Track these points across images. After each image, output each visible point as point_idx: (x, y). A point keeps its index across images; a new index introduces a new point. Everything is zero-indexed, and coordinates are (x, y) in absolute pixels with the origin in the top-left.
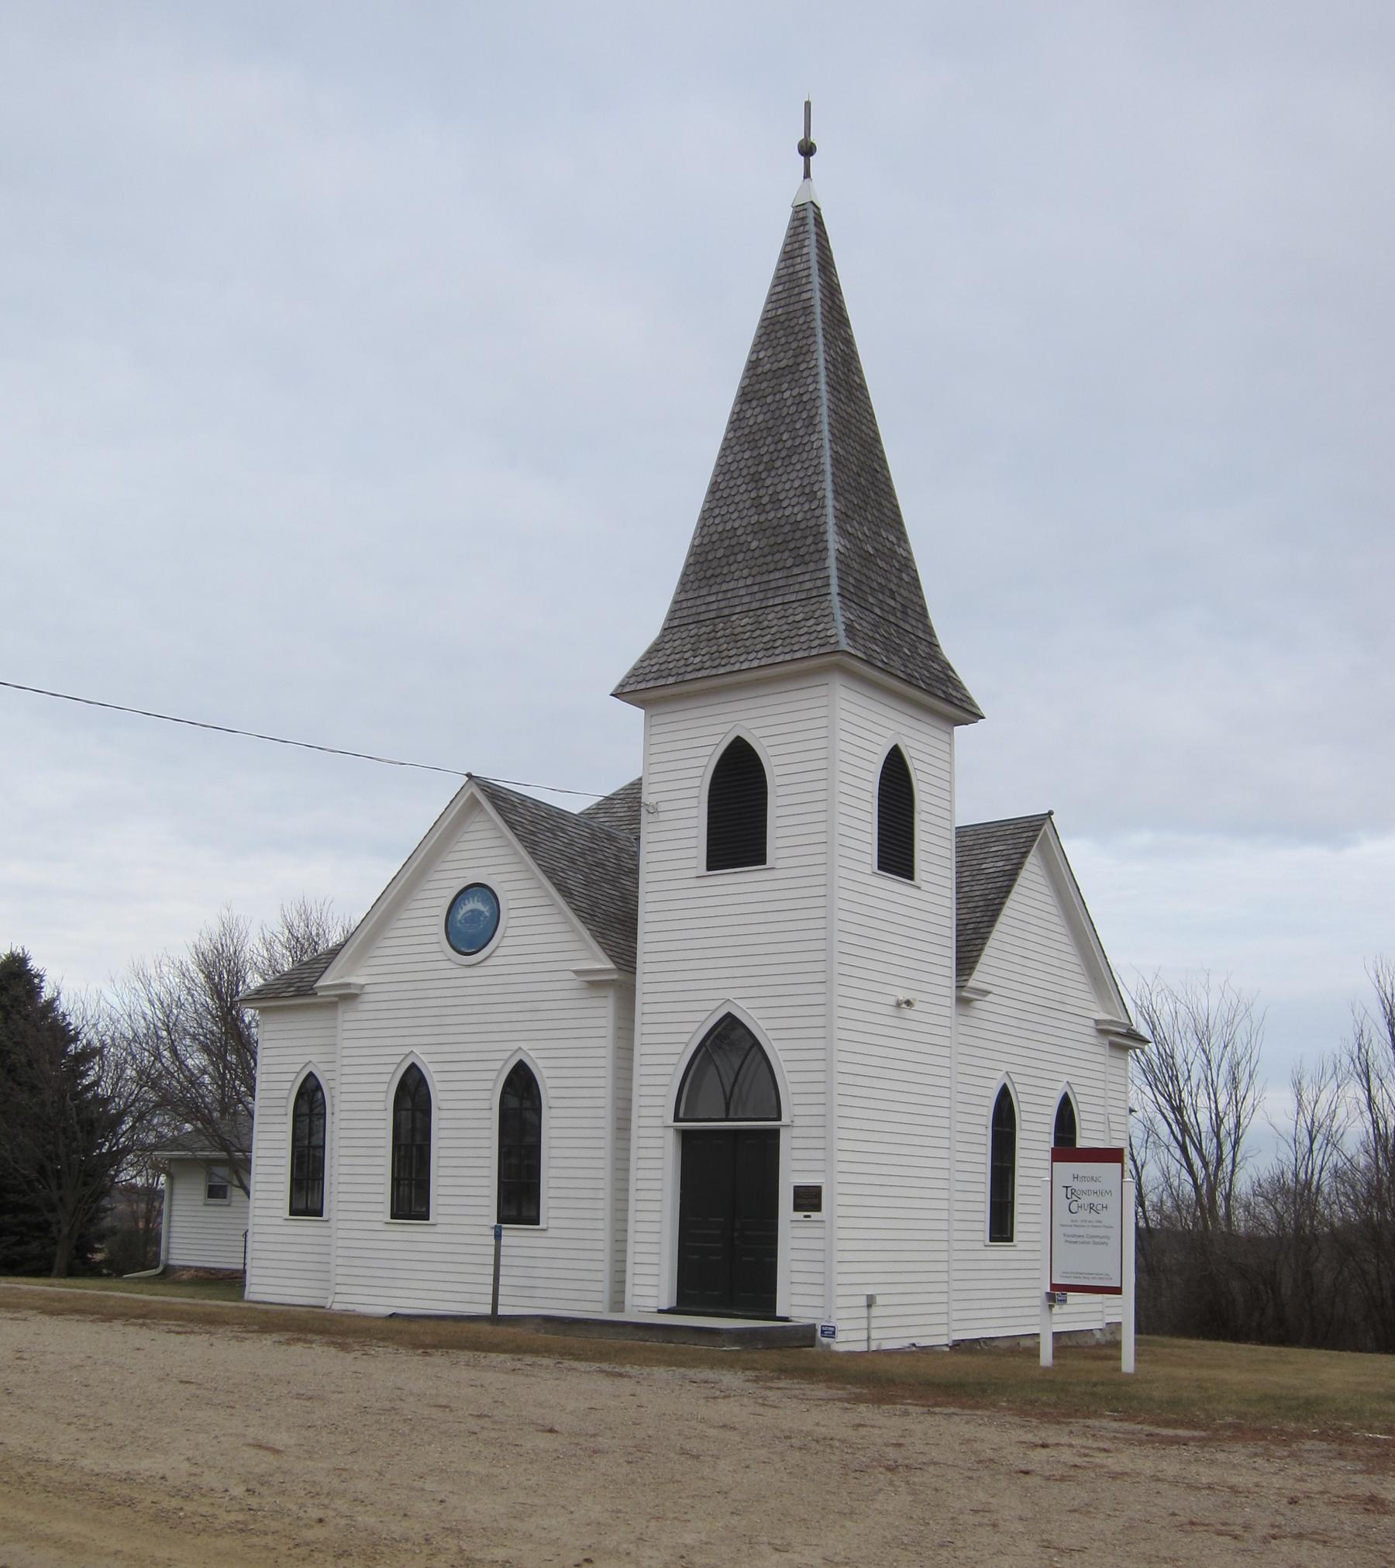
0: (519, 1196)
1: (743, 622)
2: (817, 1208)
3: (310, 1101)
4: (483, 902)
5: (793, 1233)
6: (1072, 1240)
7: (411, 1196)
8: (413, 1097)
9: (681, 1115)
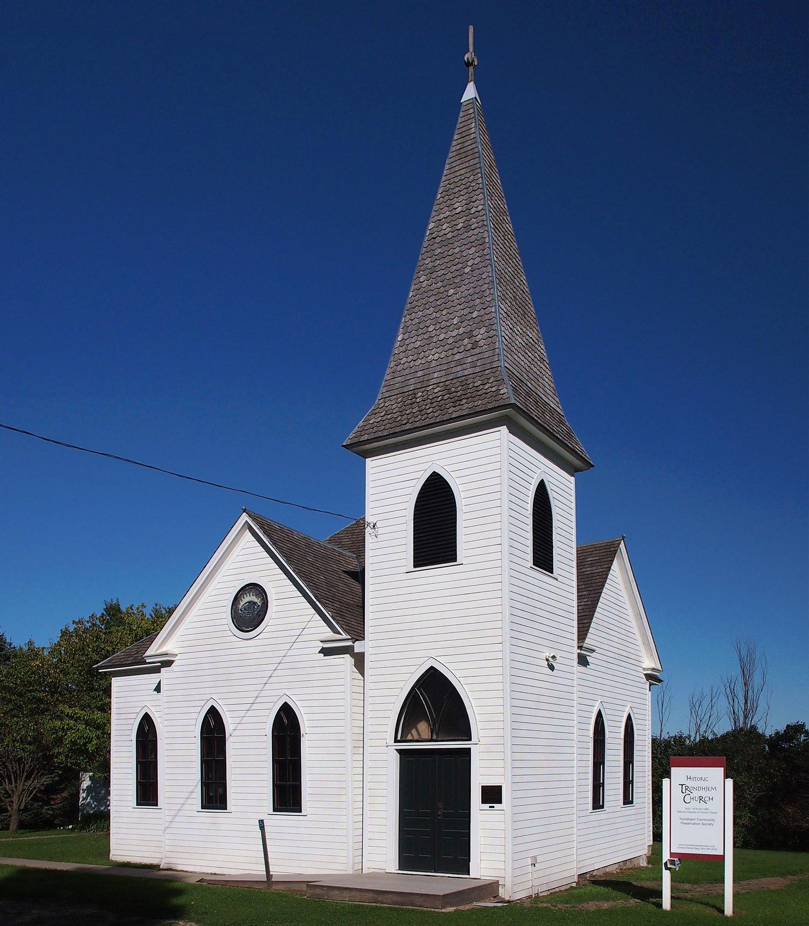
0: (287, 794)
1: (436, 391)
2: (499, 801)
3: (147, 734)
4: (256, 596)
5: (481, 816)
6: (686, 822)
7: (214, 795)
8: (213, 732)
9: (399, 738)
